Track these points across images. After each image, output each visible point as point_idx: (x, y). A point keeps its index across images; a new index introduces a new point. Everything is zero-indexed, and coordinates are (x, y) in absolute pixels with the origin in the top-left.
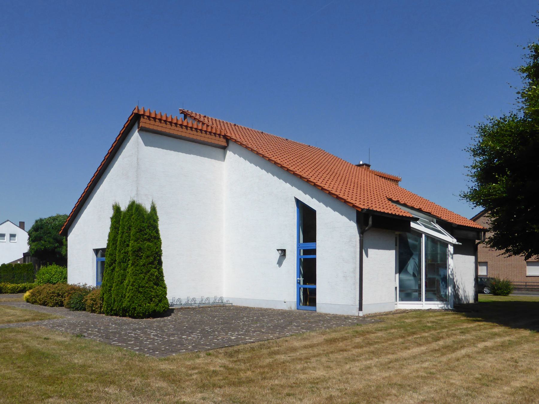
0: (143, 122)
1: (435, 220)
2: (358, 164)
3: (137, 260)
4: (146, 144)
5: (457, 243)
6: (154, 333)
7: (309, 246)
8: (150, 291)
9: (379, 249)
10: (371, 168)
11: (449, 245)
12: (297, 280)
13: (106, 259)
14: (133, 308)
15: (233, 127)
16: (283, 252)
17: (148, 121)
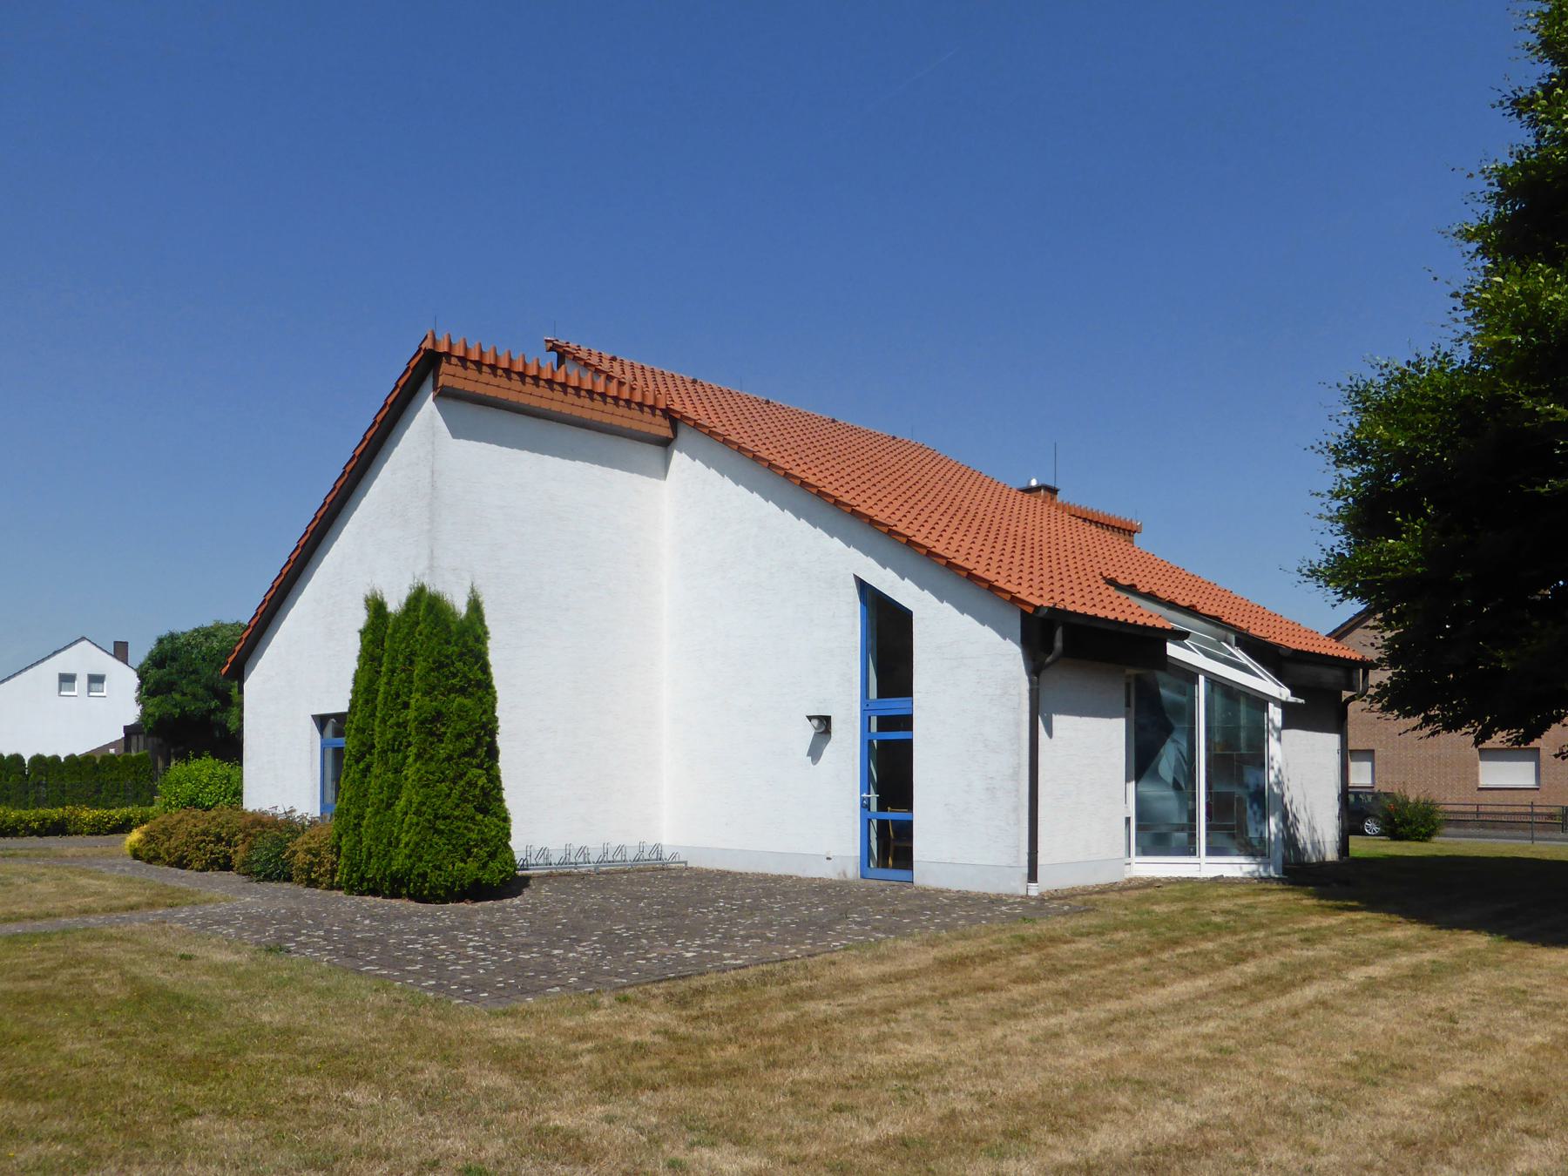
0: (449, 374)
1: (1232, 638)
2: (1024, 485)
4: (456, 434)
5: (1292, 700)
6: (476, 941)
7: (894, 706)
10: (1059, 498)
12: (863, 799)
13: (348, 741)
14: (419, 875)
17: (460, 371)
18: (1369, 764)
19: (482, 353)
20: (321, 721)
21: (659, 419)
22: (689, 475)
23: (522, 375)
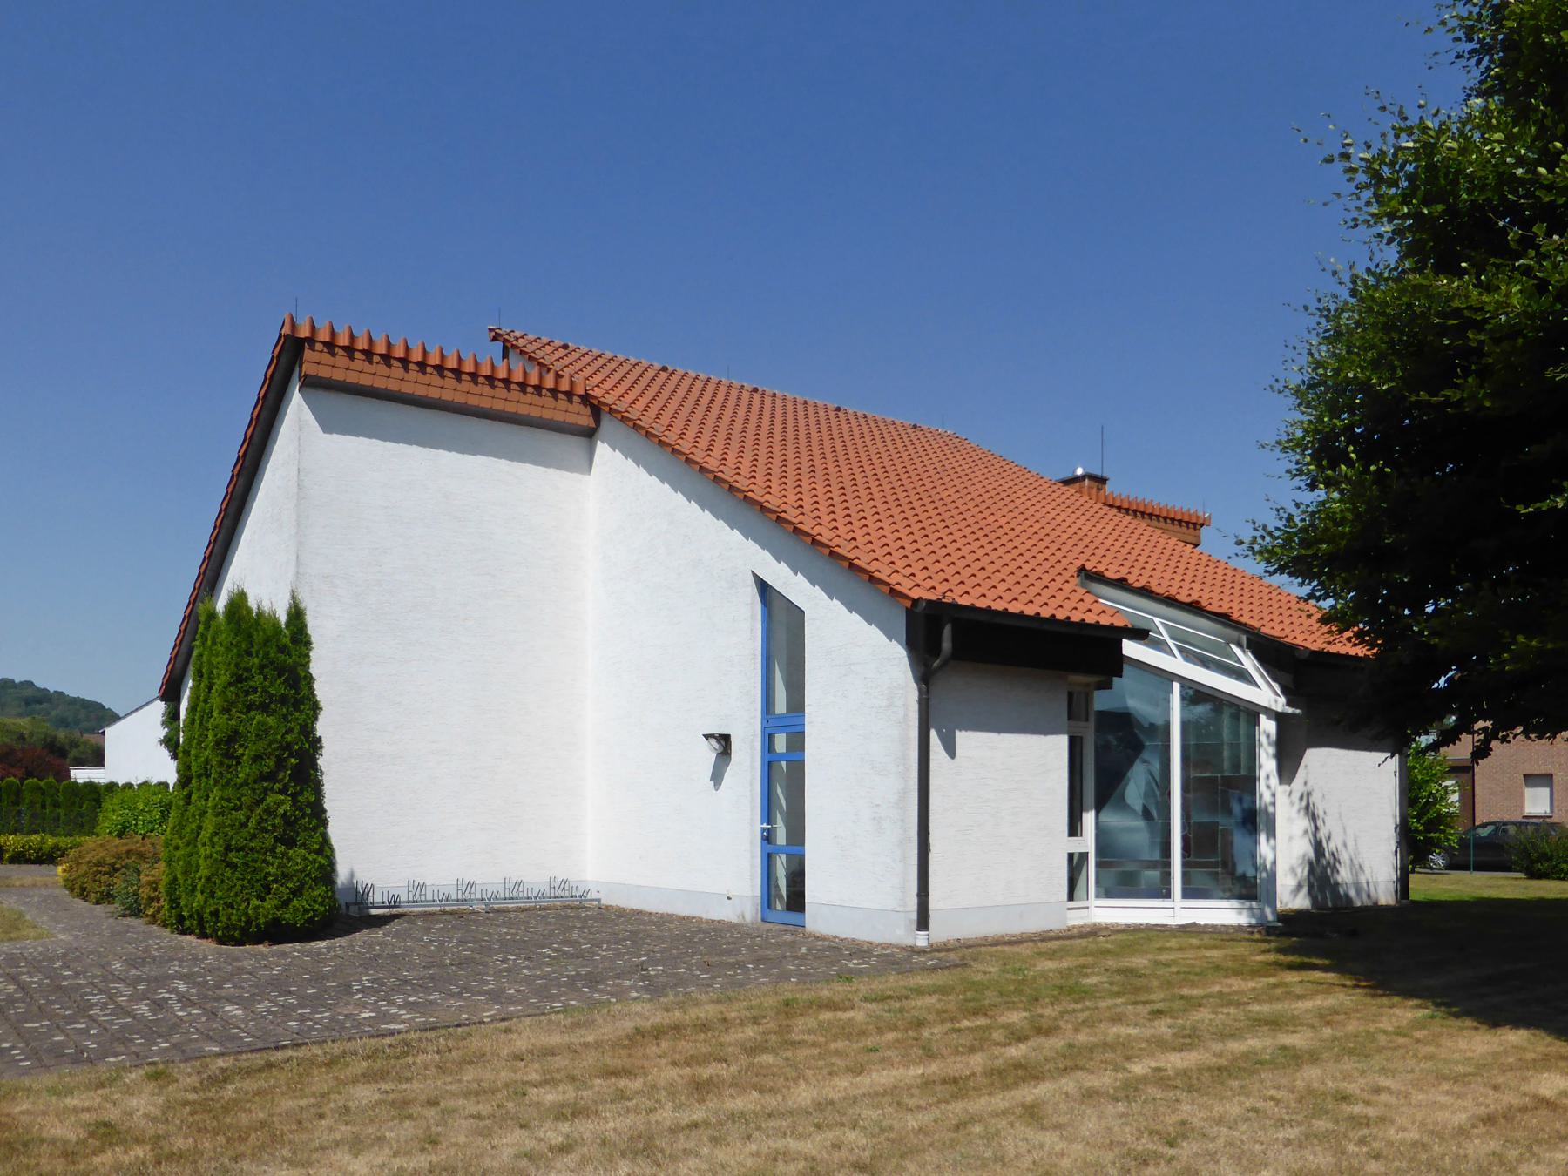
0: (314, 362)
1: (1244, 638)
2: (1067, 475)
3: (229, 767)
4: (327, 427)
5: (1290, 710)
8: (264, 861)
9: (999, 730)
10: (1108, 488)
11: (1262, 718)
12: (763, 830)
14: (211, 913)
15: (832, 414)
16: (725, 740)
17: (326, 357)
18: (1546, 791)
19: (352, 337)
20: (161, 742)
21: (577, 406)
22: (613, 467)
23: (405, 362)
